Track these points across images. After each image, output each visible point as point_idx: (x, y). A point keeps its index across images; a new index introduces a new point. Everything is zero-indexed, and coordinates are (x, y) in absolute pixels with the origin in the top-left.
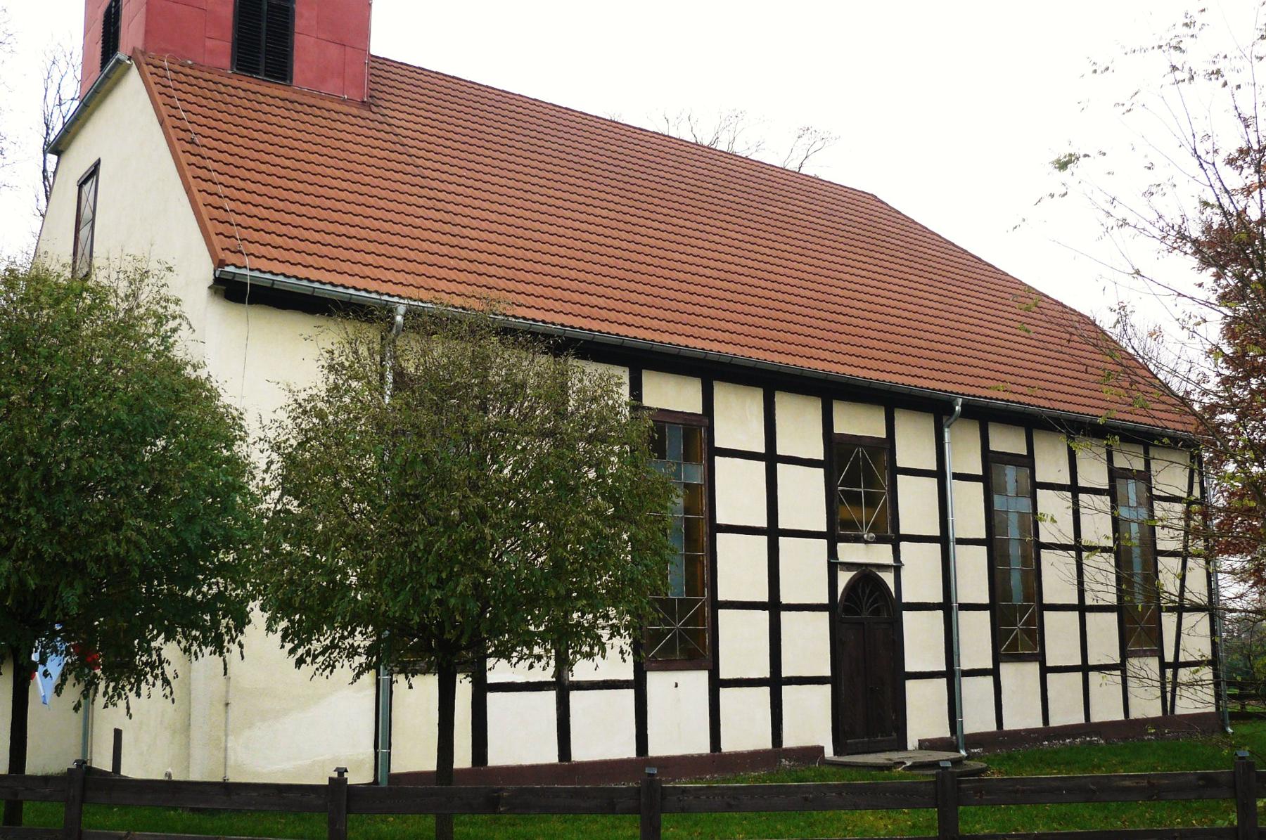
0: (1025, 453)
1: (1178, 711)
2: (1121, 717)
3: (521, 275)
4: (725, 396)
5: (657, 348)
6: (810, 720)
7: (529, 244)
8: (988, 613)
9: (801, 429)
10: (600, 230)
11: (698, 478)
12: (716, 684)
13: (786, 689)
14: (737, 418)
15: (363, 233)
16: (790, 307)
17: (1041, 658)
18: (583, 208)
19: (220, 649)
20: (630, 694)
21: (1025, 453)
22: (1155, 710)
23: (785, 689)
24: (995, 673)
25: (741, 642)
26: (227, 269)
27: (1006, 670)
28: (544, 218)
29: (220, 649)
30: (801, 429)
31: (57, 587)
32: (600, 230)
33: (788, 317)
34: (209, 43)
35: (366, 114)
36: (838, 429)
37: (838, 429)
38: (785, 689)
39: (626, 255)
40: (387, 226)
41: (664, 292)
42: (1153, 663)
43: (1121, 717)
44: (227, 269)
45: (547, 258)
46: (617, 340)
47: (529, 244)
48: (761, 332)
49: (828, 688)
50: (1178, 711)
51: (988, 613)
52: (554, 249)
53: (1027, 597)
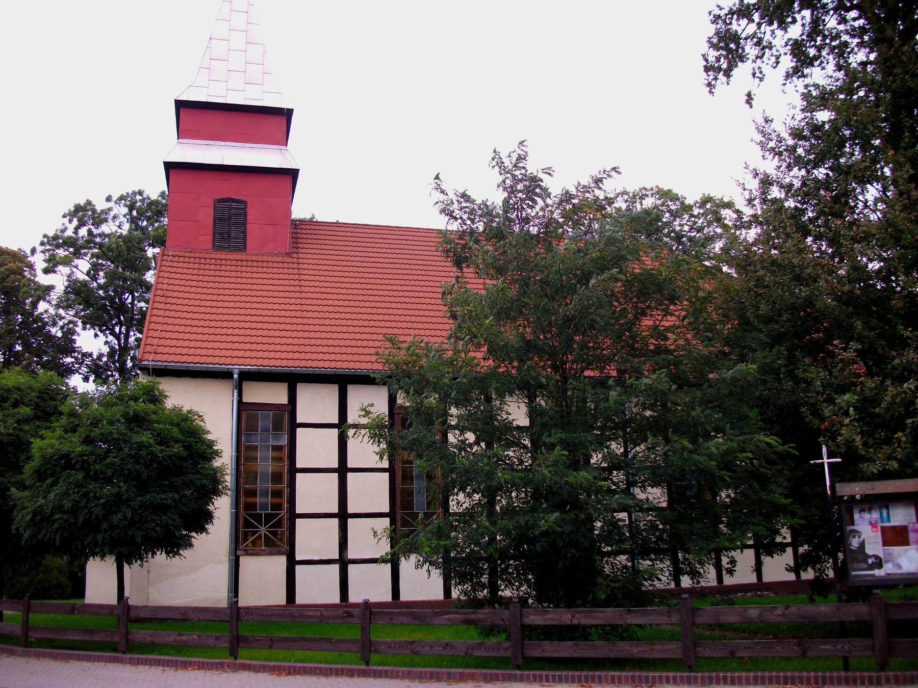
3: (278, 340)
7: (265, 333)
10: (295, 334)
11: (284, 441)
12: (292, 563)
13: (350, 521)
14: (316, 404)
15: (196, 316)
16: (266, 355)
19: (142, 560)
23: (350, 521)
28: (362, 330)
29: (142, 560)
31: (113, 333)
32: (295, 334)
34: (201, 238)
35: (290, 260)
38: (350, 521)
39: (355, 350)
40: (184, 315)
45: (201, 330)
47: (265, 333)
52: (224, 331)
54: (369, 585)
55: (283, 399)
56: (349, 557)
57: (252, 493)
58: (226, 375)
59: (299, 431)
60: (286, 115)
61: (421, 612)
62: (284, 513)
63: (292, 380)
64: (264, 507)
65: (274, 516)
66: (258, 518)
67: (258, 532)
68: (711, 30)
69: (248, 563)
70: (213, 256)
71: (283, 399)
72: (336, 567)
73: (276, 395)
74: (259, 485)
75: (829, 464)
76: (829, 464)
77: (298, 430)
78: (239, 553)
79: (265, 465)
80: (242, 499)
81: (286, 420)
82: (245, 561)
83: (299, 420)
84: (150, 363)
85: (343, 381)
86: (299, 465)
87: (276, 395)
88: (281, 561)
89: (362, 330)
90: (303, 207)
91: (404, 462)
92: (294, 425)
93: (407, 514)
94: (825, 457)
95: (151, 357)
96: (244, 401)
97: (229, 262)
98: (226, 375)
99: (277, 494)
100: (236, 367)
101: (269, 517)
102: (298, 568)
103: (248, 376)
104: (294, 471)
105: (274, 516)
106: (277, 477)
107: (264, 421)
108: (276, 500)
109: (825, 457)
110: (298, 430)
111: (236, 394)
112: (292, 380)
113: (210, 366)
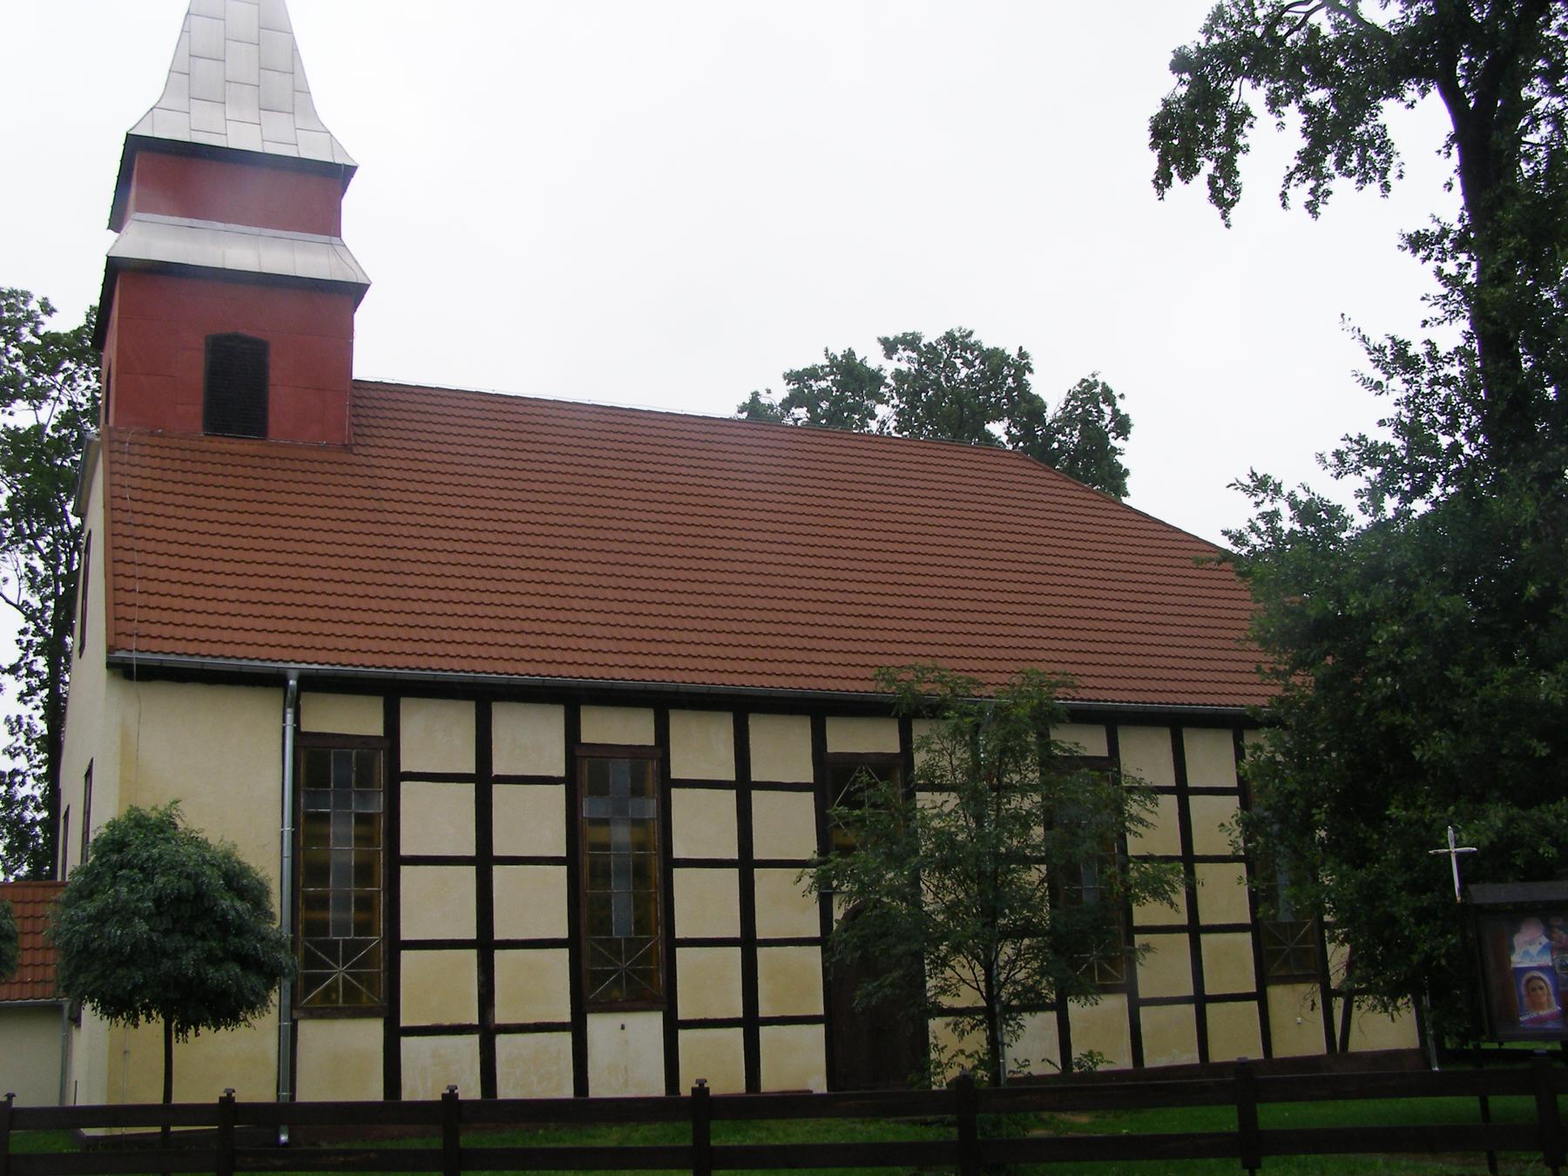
0: (1106, 754)
1: (1355, 1045)
2: (1193, 1057)
4: (762, 731)
5: (682, 687)
6: (798, 1060)
8: (566, 951)
9: (783, 750)
11: (378, 805)
12: (673, 1026)
14: (701, 747)
15: (431, 621)
17: (1130, 989)
18: (483, 537)
20: (566, 1038)
21: (1106, 754)
22: (1316, 1045)
24: (1260, 997)
25: (707, 981)
26: (117, 654)
27: (1276, 993)
30: (783, 750)
33: (1187, 675)
36: (832, 747)
37: (832, 747)
41: (500, 611)
42: (1311, 990)
43: (1193, 1057)
44: (117, 654)
46: (703, 688)
48: (730, 652)
49: (821, 1028)
50: (1355, 1045)
51: (566, 951)
53: (641, 925)
54: (1235, 1036)
55: (376, 728)
56: (497, 1021)
57: (321, 902)
58: (274, 680)
59: (405, 786)
60: (338, 175)
61: (1384, 1073)
62: (376, 939)
63: (393, 692)
64: (342, 928)
65: (360, 945)
66: (330, 949)
67: (330, 975)
68: (1395, 148)
69: (600, 1026)
70: (205, 445)
71: (376, 728)
72: (474, 1039)
73: (635, 729)
74: (333, 887)
75: (1459, 855)
76: (1459, 855)
77: (404, 785)
78: (296, 1015)
79: (342, 849)
80: (302, 914)
81: (652, 772)
82: (307, 1029)
83: (405, 767)
84: (135, 655)
85: (742, 707)
86: (405, 850)
87: (635, 729)
88: (372, 1032)
89: (339, 588)
90: (373, 359)
91: (594, 846)
92: (396, 777)
93: (600, 942)
94: (1452, 845)
95: (133, 643)
96: (304, 729)
97: (217, 458)
98: (274, 680)
99: (365, 904)
100: (293, 665)
101: (352, 948)
102: (406, 1043)
103: (315, 683)
104: (396, 861)
105: (360, 945)
106: (364, 873)
107: (620, 775)
108: (317, 915)
109: (1452, 845)
110: (404, 785)
111: (290, 717)
112: (393, 692)
113: (245, 662)
